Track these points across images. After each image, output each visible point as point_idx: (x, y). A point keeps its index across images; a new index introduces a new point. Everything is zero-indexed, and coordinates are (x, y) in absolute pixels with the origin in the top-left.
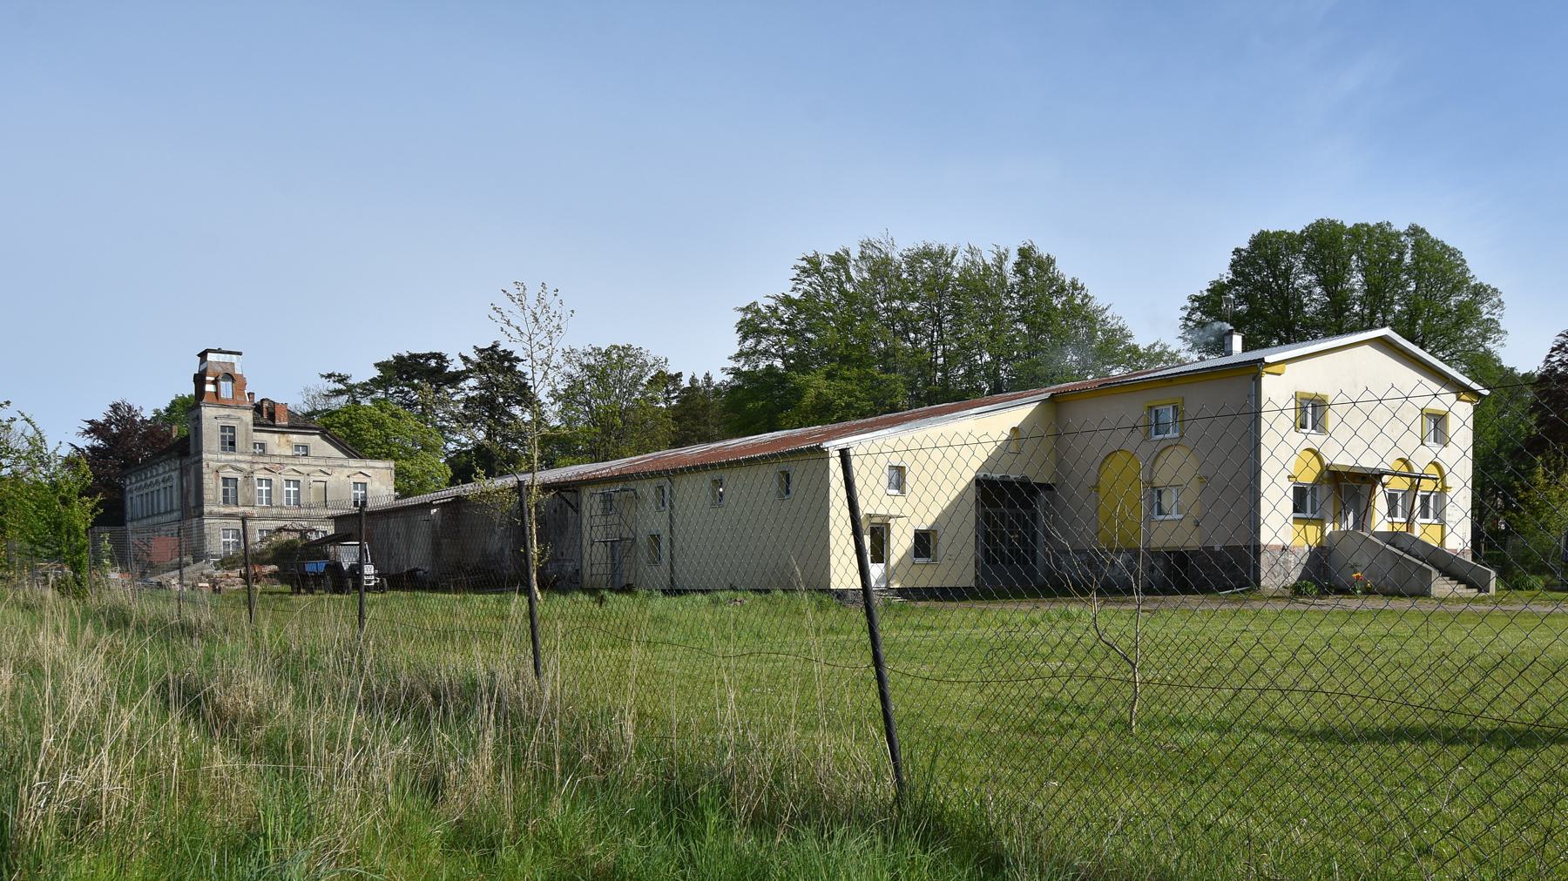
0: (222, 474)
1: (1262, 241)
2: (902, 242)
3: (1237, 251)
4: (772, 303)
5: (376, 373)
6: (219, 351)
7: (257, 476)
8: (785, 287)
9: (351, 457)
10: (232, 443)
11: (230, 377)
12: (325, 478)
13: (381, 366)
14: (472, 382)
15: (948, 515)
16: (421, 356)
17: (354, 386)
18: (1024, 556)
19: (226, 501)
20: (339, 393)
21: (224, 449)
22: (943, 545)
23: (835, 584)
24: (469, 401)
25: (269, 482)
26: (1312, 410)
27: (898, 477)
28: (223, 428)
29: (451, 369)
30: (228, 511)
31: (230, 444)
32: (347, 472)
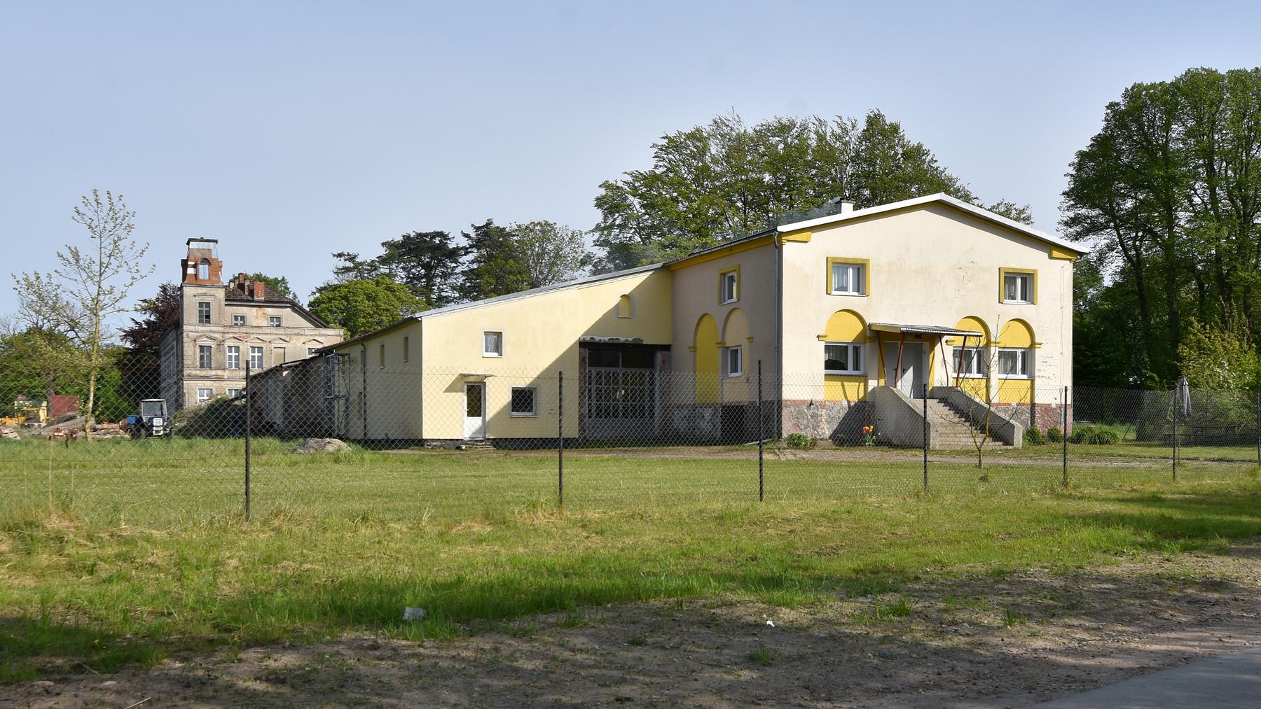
0: (199, 343)
1: (1136, 95)
2: (751, 119)
3: (1112, 106)
4: (630, 179)
5: (383, 252)
6: (202, 240)
7: (227, 344)
8: (647, 164)
9: (317, 327)
10: (208, 317)
11: (206, 261)
12: (284, 345)
13: (389, 245)
14: (471, 257)
15: (556, 373)
16: (426, 235)
17: (361, 264)
18: (639, 409)
19: (202, 366)
20: (347, 270)
21: (201, 321)
22: (545, 401)
23: (430, 431)
24: (469, 274)
25: (237, 349)
26: (854, 273)
27: (495, 341)
28: (201, 304)
29: (452, 245)
30: (203, 373)
31: (206, 318)
32: (303, 339)
